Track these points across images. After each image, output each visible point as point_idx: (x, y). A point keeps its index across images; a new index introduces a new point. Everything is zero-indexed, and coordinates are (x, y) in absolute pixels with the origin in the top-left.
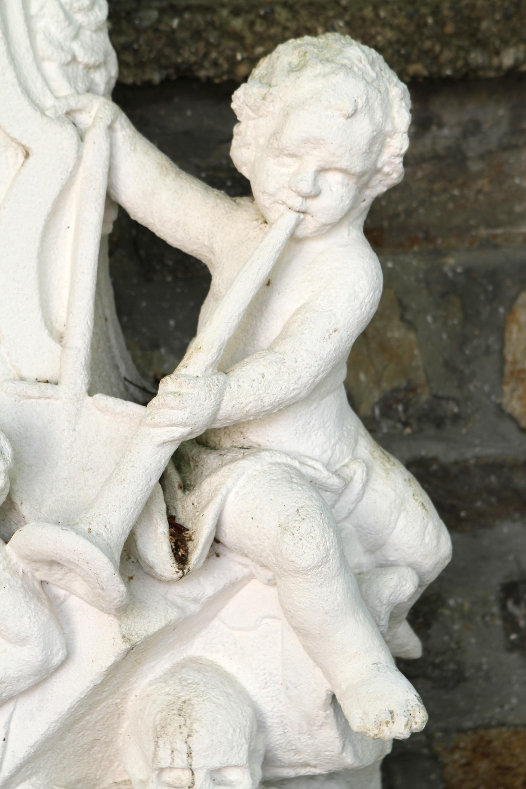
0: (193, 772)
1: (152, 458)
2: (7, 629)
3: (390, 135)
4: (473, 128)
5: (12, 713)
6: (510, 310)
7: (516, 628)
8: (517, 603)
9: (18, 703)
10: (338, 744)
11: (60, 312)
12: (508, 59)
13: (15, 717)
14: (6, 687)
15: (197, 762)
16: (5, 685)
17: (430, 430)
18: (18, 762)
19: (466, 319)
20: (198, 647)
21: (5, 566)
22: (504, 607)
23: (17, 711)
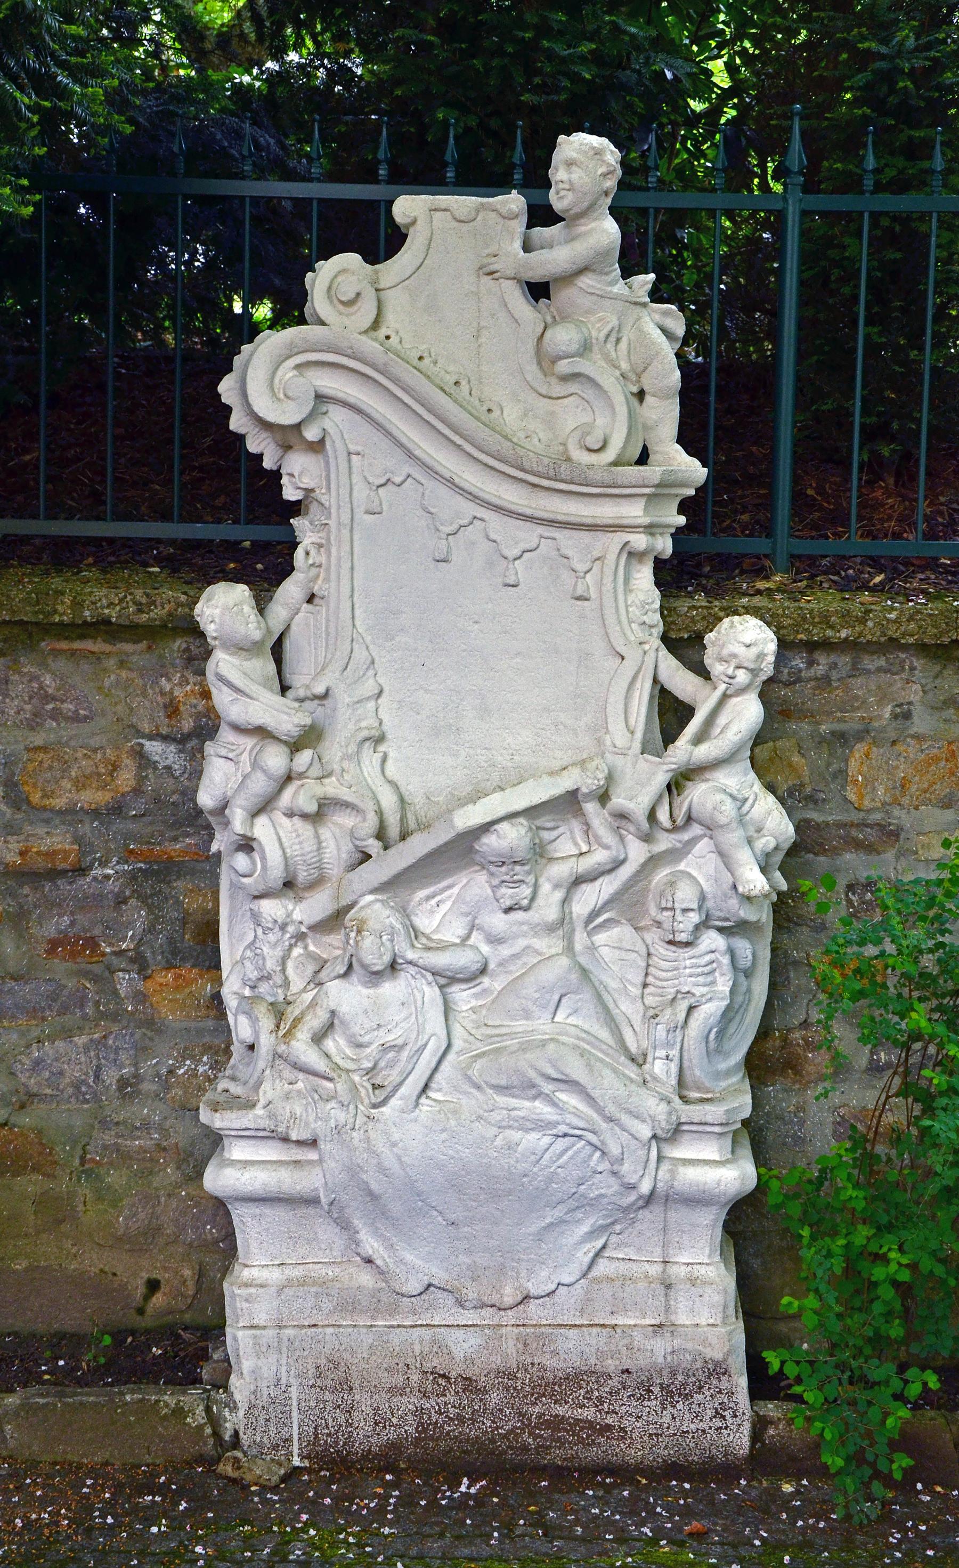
1: (661, 778)
3: (766, 655)
4: (834, 666)
6: (851, 751)
7: (853, 907)
8: (854, 894)
10: (737, 906)
11: (632, 721)
12: (843, 634)
15: (676, 905)
17: (811, 806)
19: (830, 755)
20: (682, 866)
22: (847, 895)
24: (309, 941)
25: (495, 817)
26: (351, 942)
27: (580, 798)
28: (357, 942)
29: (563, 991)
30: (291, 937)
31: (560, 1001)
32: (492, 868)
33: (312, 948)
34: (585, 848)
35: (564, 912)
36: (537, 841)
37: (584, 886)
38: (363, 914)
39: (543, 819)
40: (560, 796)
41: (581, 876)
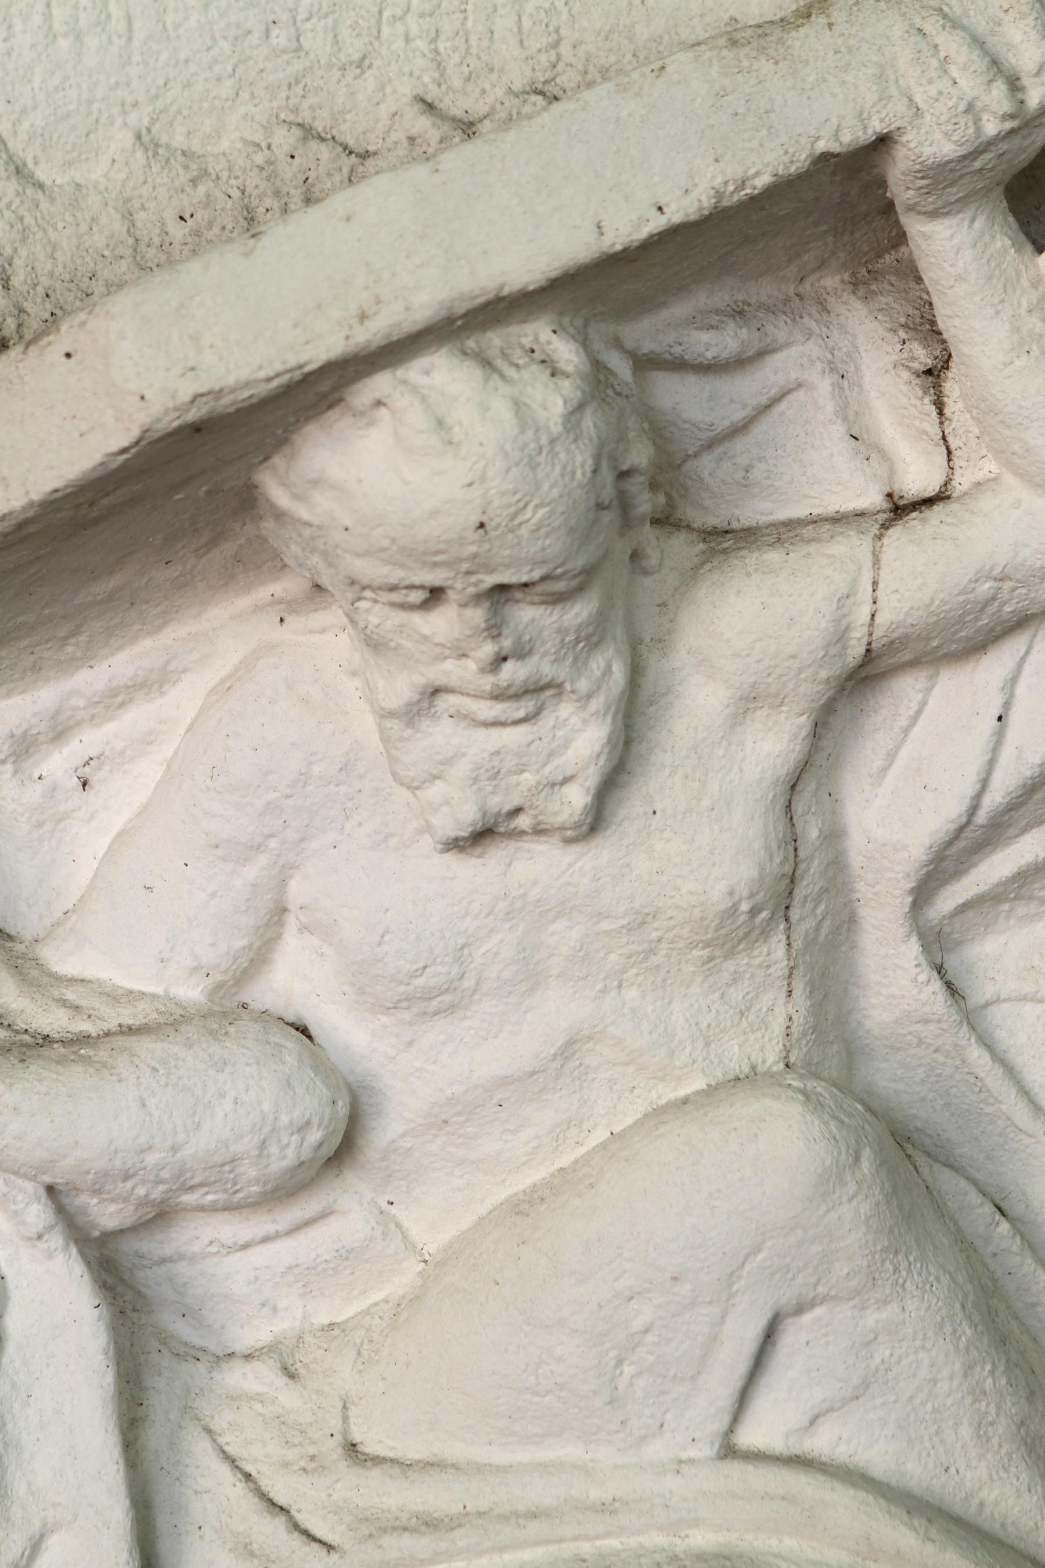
0: (949, 453)
2: (1027, 451)
5: (1013, 680)
9: (1037, 639)
13: (1028, 669)
14: (1014, 589)
16: (1011, 584)
18: (1028, 774)
21: (1034, 302)
23: (1033, 658)
25: (368, 335)
27: (902, 188)
29: (787, 1296)
31: (770, 1336)
32: (377, 615)
34: (919, 477)
35: (793, 841)
36: (639, 455)
37: (907, 689)
39: (680, 309)
40: (783, 189)
41: (892, 646)
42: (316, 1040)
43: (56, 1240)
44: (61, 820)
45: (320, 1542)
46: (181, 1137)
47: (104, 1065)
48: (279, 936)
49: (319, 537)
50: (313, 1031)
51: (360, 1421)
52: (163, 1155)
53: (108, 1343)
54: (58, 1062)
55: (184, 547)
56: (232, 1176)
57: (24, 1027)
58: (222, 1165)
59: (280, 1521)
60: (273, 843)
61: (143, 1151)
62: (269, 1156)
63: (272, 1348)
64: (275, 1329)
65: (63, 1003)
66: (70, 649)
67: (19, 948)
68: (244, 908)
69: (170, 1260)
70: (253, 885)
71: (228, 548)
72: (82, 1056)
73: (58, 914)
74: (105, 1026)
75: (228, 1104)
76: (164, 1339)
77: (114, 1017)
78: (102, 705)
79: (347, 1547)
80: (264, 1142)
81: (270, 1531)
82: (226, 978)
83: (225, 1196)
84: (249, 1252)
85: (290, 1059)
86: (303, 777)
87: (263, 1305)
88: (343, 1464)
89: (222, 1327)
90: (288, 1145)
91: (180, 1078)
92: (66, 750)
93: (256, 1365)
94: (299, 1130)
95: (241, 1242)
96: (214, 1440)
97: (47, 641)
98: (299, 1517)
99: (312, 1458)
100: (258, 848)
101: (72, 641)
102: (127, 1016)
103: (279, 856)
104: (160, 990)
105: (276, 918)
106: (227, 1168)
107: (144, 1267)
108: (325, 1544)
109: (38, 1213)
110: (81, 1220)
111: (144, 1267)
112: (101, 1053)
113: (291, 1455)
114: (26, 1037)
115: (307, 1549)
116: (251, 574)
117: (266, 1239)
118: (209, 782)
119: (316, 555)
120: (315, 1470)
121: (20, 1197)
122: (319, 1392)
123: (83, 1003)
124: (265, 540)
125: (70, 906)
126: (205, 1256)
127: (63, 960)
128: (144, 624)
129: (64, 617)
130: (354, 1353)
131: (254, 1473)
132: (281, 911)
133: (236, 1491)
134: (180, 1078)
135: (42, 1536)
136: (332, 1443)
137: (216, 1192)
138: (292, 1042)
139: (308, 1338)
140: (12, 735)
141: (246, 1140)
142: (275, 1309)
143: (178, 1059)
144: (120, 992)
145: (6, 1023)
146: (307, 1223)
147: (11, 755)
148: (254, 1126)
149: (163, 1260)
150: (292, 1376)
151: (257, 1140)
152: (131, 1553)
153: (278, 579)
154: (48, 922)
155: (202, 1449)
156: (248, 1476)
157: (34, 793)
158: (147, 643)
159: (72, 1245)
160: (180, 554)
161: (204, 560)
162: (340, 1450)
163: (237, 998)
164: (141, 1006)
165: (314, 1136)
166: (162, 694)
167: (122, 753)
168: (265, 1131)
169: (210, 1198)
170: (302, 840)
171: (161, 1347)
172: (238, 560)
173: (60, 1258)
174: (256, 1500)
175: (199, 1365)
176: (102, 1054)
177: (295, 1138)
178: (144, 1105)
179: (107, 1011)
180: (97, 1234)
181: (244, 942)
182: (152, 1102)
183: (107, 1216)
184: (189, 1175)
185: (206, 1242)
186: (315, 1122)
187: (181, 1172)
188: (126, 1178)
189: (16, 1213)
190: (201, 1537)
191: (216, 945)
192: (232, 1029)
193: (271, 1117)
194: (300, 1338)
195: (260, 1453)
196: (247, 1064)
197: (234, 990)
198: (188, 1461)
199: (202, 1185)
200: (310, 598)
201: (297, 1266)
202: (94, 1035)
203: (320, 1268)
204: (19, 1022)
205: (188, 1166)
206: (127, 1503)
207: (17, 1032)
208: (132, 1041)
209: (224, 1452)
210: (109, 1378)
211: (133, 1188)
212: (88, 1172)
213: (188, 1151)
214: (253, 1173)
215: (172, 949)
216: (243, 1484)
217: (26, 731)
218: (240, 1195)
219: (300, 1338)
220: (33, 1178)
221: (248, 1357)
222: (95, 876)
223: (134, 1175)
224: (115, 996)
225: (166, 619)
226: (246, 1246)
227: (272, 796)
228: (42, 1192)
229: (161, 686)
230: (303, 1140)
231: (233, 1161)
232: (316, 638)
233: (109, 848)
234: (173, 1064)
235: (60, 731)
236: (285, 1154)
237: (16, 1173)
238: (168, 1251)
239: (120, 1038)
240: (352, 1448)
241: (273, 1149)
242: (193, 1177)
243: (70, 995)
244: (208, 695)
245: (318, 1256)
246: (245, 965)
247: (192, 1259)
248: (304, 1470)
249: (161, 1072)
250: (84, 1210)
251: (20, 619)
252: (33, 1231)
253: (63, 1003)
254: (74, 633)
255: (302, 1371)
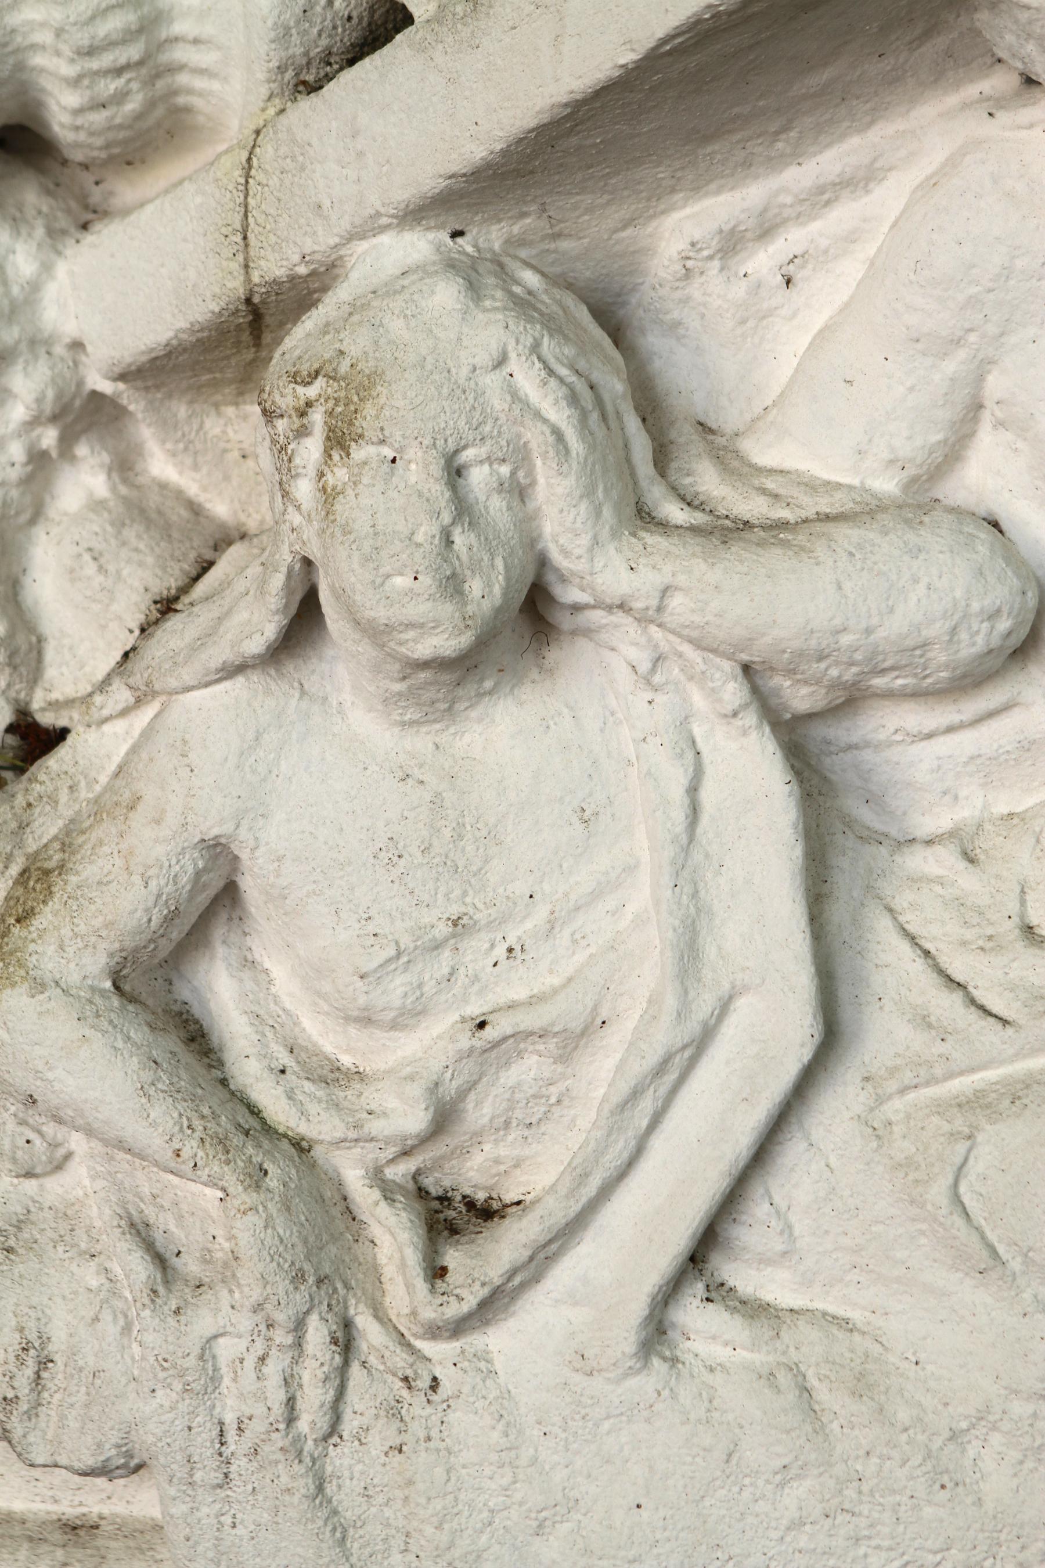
24: (146, 433)
26: (304, 489)
28: (328, 495)
30: (34, 422)
33: (160, 465)
38: (357, 344)
42: (1007, 534)
43: (750, 718)
44: (764, 317)
45: (996, 1016)
46: (875, 621)
47: (802, 548)
48: (972, 434)
49: (1037, 20)
50: (1004, 527)
51: (1038, 905)
52: (857, 636)
53: (798, 819)
54: (758, 545)
55: (898, 39)
56: (922, 660)
57: (725, 513)
58: (914, 649)
59: (958, 997)
60: (972, 338)
61: (838, 632)
62: (959, 642)
63: (953, 834)
64: (955, 817)
65: (763, 491)
66: (780, 145)
67: (721, 441)
68: (941, 403)
69: (855, 747)
70: (951, 379)
71: (940, 42)
72: (782, 540)
73: (758, 410)
74: (804, 514)
75: (921, 589)
76: (849, 823)
77: (812, 505)
78: (808, 203)
79: (1022, 1022)
80: (955, 629)
81: (948, 1006)
82: (920, 472)
83: (914, 681)
84: (933, 741)
85: (983, 549)
86: (1005, 272)
87: (945, 793)
88: (1020, 945)
89: (905, 814)
90: (978, 632)
91: (875, 563)
92: (771, 249)
93: (938, 849)
94: (990, 618)
95: (926, 731)
96: (895, 919)
97: (759, 136)
98: (976, 993)
99: (990, 938)
100: (957, 342)
101: (783, 136)
102: (824, 505)
103: (978, 350)
104: (856, 482)
105: (972, 415)
106: (918, 652)
107: (831, 753)
108: (1001, 1019)
109: (733, 691)
110: (773, 702)
111: (831, 753)
112: (800, 537)
113: (969, 934)
114: (727, 522)
115: (983, 1023)
116: (961, 70)
117: (950, 729)
118: (912, 277)
119: (1032, 42)
120: (992, 949)
121: (717, 675)
122: (998, 877)
123: (782, 491)
124: (979, 33)
125: (769, 402)
126: (890, 744)
127: (763, 452)
128: (853, 121)
129: (777, 110)
130: (1033, 840)
131: (933, 951)
132: (976, 407)
133: (918, 966)
134: (875, 563)
135: (731, 998)
136: (1009, 924)
137: (906, 676)
138: (985, 534)
139: (988, 826)
140: (721, 231)
141: (938, 625)
142: (956, 798)
143: (874, 545)
144: (818, 482)
145: (708, 509)
146: (991, 715)
147: (719, 251)
148: (946, 612)
149: (850, 747)
150: (972, 861)
151: (948, 625)
152: (815, 1017)
153: (987, 76)
154: (748, 417)
155: (883, 927)
156: (927, 953)
157: (739, 290)
158: (854, 141)
159: (765, 723)
160: (894, 46)
161: (916, 54)
162: (1017, 931)
163: (929, 494)
164: (838, 495)
165: (1004, 625)
166: (868, 192)
167: (826, 252)
168: (956, 617)
169: (900, 682)
170: (1002, 334)
171: (846, 830)
172: (949, 54)
173: (754, 735)
174: (935, 975)
175: (881, 848)
176: (801, 538)
177: (986, 625)
178: (840, 588)
179: (806, 500)
180: (788, 716)
181: (940, 437)
182: (847, 586)
183: (800, 698)
184: (881, 657)
185: (892, 730)
186: (1005, 610)
187: (875, 653)
188: (821, 659)
189: (713, 690)
190: (881, 1008)
191: (914, 439)
192: (926, 519)
193: (963, 603)
194: (980, 826)
195: (941, 932)
196: (941, 552)
197: (926, 486)
198: (869, 936)
199: (892, 668)
200: (1018, 94)
201: (979, 756)
202: (792, 522)
203: (1002, 758)
204: (720, 508)
205: (880, 649)
206: (813, 970)
207: (718, 517)
208: (830, 527)
209: (904, 930)
210: (798, 851)
211: (826, 669)
212: (784, 652)
213: (881, 634)
214: (943, 658)
215: (870, 441)
216: (923, 960)
217: (735, 227)
218: (929, 680)
219: (980, 826)
220: (730, 658)
221: (929, 842)
222: (797, 370)
223: (827, 656)
224: (813, 486)
225: (874, 117)
226: (930, 736)
227: (974, 290)
228: (739, 671)
229: (866, 185)
230: (992, 627)
231: (925, 645)
232: (1024, 133)
233: (811, 344)
234: (869, 549)
235: (766, 229)
236: (976, 641)
237: (714, 651)
238: (855, 738)
239: (818, 524)
240: (1029, 930)
241: (964, 636)
242: (884, 660)
243: (770, 484)
244: (914, 192)
245: (1000, 747)
246: (940, 460)
247: (878, 747)
248: (982, 949)
249: (858, 556)
250: (777, 692)
251: (736, 110)
252: (729, 709)
253: (763, 491)
254: (785, 129)
255: (982, 857)
